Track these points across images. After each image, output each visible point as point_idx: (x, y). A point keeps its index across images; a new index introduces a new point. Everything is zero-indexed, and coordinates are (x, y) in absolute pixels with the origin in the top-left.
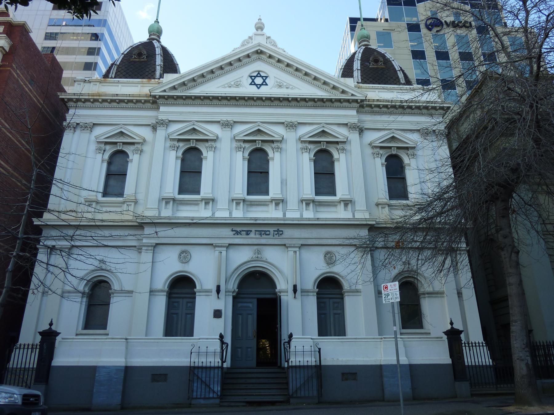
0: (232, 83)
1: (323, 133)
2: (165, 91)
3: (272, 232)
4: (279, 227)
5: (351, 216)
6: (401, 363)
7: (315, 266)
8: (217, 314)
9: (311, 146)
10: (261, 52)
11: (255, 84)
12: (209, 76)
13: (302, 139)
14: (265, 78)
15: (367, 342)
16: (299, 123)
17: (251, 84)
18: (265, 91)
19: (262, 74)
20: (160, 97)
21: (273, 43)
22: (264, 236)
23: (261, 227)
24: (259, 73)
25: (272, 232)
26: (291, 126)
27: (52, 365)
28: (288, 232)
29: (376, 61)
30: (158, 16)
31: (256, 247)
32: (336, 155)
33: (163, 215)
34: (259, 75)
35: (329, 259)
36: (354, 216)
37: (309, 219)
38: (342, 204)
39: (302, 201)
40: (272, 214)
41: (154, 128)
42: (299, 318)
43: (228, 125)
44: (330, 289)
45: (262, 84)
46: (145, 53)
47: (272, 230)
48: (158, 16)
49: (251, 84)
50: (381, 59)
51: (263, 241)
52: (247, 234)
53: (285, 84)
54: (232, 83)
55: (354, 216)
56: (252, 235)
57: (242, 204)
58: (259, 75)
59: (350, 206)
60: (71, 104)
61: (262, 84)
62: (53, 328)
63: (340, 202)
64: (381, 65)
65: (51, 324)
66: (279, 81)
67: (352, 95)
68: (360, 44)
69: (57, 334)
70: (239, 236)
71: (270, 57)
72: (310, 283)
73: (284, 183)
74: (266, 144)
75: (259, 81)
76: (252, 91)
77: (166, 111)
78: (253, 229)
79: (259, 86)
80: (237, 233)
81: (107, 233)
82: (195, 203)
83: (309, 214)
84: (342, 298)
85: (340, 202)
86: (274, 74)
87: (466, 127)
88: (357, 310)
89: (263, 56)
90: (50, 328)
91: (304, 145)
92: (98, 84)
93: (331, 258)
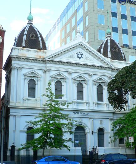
2: (49, 58)
3: (85, 113)
4: (87, 112)
5: (108, 110)
7: (98, 126)
9: (97, 83)
10: (81, 45)
11: (78, 55)
14: (82, 55)
15: (109, 148)
17: (82, 58)
18: (82, 61)
19: (81, 54)
20: (48, 60)
22: (83, 115)
23: (82, 112)
25: (85, 113)
26: (70, 73)
28: (90, 114)
29: (116, 49)
30: (30, 11)
31: (80, 118)
33: (95, 109)
34: (80, 54)
36: (73, 108)
37: (75, 109)
38: (106, 105)
40: (85, 107)
41: (45, 72)
43: (70, 73)
44: (101, 131)
45: (79, 58)
46: (35, 35)
47: (85, 113)
48: (30, 11)
49: (82, 58)
50: (117, 48)
51: (82, 116)
52: (78, 114)
55: (73, 108)
56: (79, 114)
57: (97, 105)
59: (88, 104)
60: (13, 59)
61: (79, 58)
62: (14, 145)
64: (117, 51)
65: (13, 144)
67: (110, 66)
68: (107, 35)
69: (15, 146)
70: (75, 114)
72: (96, 131)
73: (88, 96)
74: (83, 81)
76: (77, 61)
77: (49, 66)
78: (80, 112)
79: (80, 58)
80: (75, 113)
81: (21, 111)
82: (83, 103)
83: (96, 108)
84: (104, 135)
88: (108, 138)
92: (21, 50)
93: (102, 122)
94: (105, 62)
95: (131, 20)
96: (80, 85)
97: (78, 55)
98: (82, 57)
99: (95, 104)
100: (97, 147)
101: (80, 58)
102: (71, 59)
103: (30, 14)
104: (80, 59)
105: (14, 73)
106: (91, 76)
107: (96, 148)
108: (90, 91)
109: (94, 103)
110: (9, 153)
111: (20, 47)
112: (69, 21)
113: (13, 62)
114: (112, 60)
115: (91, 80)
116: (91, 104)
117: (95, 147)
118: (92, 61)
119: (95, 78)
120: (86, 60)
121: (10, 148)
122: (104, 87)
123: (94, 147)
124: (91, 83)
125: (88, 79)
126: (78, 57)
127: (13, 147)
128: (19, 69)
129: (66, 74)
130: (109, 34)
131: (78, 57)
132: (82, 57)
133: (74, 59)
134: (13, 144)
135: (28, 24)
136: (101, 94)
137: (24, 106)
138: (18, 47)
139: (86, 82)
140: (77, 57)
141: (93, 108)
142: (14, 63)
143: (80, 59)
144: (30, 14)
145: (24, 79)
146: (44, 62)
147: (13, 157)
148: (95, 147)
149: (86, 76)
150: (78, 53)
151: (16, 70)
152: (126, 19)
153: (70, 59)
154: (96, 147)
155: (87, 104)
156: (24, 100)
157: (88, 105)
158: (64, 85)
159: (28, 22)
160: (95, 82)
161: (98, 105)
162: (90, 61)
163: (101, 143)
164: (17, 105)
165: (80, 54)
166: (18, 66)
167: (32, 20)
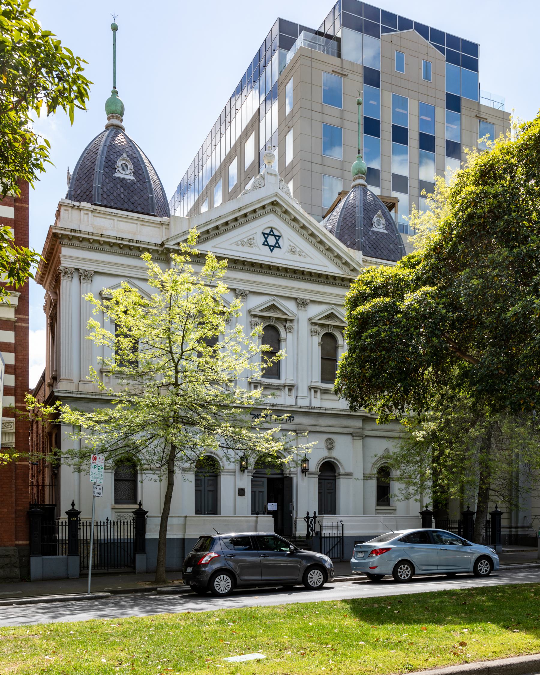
0: (246, 240)
1: (273, 307)
2: (178, 244)
6: (170, 535)
8: (242, 492)
11: (266, 238)
12: (222, 229)
13: (253, 313)
14: (278, 238)
16: (96, 273)
17: (279, 247)
18: (280, 258)
19: (276, 233)
21: (285, 190)
24: (272, 231)
26: (302, 304)
27: (168, 537)
32: (283, 334)
35: (330, 445)
38: (287, 388)
39: (250, 383)
40: (284, 399)
42: (306, 496)
44: (329, 471)
45: (270, 246)
49: (279, 247)
53: (298, 250)
54: (246, 240)
55: (296, 403)
57: (319, 392)
58: (271, 233)
61: (270, 246)
62: (76, 508)
63: (284, 387)
65: (73, 505)
66: (292, 244)
71: (286, 212)
72: (314, 466)
75: (272, 240)
76: (261, 254)
79: (272, 248)
84: (335, 480)
85: (284, 387)
86: (289, 235)
87: (366, 307)
89: (278, 209)
90: (140, 508)
91: (315, 328)
94: (346, 264)
95: (433, 138)
96: (271, 332)
97: (266, 238)
98: (277, 246)
99: (312, 391)
100: (317, 515)
101: (272, 248)
102: (246, 249)
103: (115, 93)
104: (272, 251)
105: (69, 287)
106: (302, 304)
107: (315, 517)
108: (301, 354)
109: (310, 389)
110: (63, 534)
111: (84, 204)
112: (252, 126)
113: (65, 251)
114: (367, 258)
115: (303, 317)
116: (303, 391)
117: (311, 515)
118: (307, 260)
119: (315, 311)
120: (290, 256)
121: (64, 517)
122: (340, 341)
123: (308, 513)
124: (302, 327)
125: (295, 315)
126: (268, 245)
127: (73, 514)
128: (85, 276)
129: (290, 307)
130: (117, 118)
131: (268, 245)
132: (277, 246)
133: (254, 250)
134: (73, 505)
135: (107, 127)
136: (330, 362)
137: (313, 405)
138: (77, 204)
139: (288, 324)
140: (264, 244)
141: (308, 401)
142: (69, 257)
143: (272, 251)
144: (115, 93)
145: (251, 324)
146: (163, 257)
147: (74, 545)
148: (311, 515)
149: (290, 307)
150: (268, 231)
151: (76, 280)
152: (447, 141)
153: (240, 248)
154: (315, 513)
155: (290, 390)
156: (104, 374)
157: (293, 392)
158: (285, 340)
159: (106, 122)
160: (255, 316)
161: (321, 393)
162: (301, 259)
163: (207, 502)
164: (84, 388)
165: (271, 233)
166: (83, 266)
167: (122, 114)
